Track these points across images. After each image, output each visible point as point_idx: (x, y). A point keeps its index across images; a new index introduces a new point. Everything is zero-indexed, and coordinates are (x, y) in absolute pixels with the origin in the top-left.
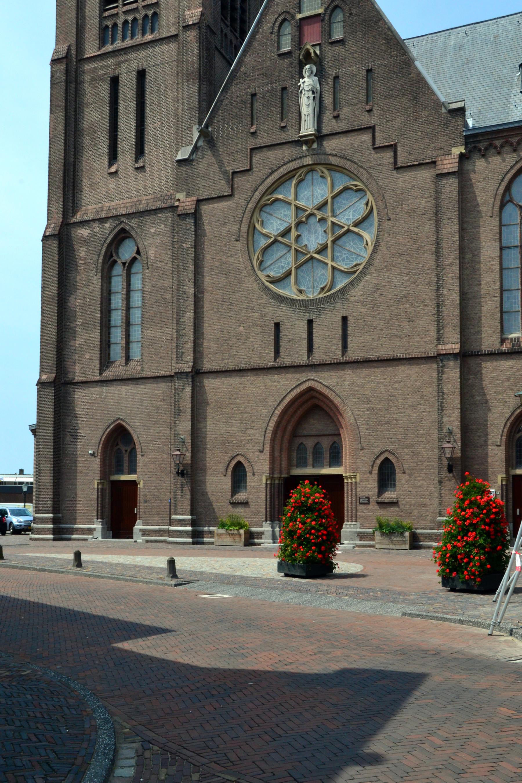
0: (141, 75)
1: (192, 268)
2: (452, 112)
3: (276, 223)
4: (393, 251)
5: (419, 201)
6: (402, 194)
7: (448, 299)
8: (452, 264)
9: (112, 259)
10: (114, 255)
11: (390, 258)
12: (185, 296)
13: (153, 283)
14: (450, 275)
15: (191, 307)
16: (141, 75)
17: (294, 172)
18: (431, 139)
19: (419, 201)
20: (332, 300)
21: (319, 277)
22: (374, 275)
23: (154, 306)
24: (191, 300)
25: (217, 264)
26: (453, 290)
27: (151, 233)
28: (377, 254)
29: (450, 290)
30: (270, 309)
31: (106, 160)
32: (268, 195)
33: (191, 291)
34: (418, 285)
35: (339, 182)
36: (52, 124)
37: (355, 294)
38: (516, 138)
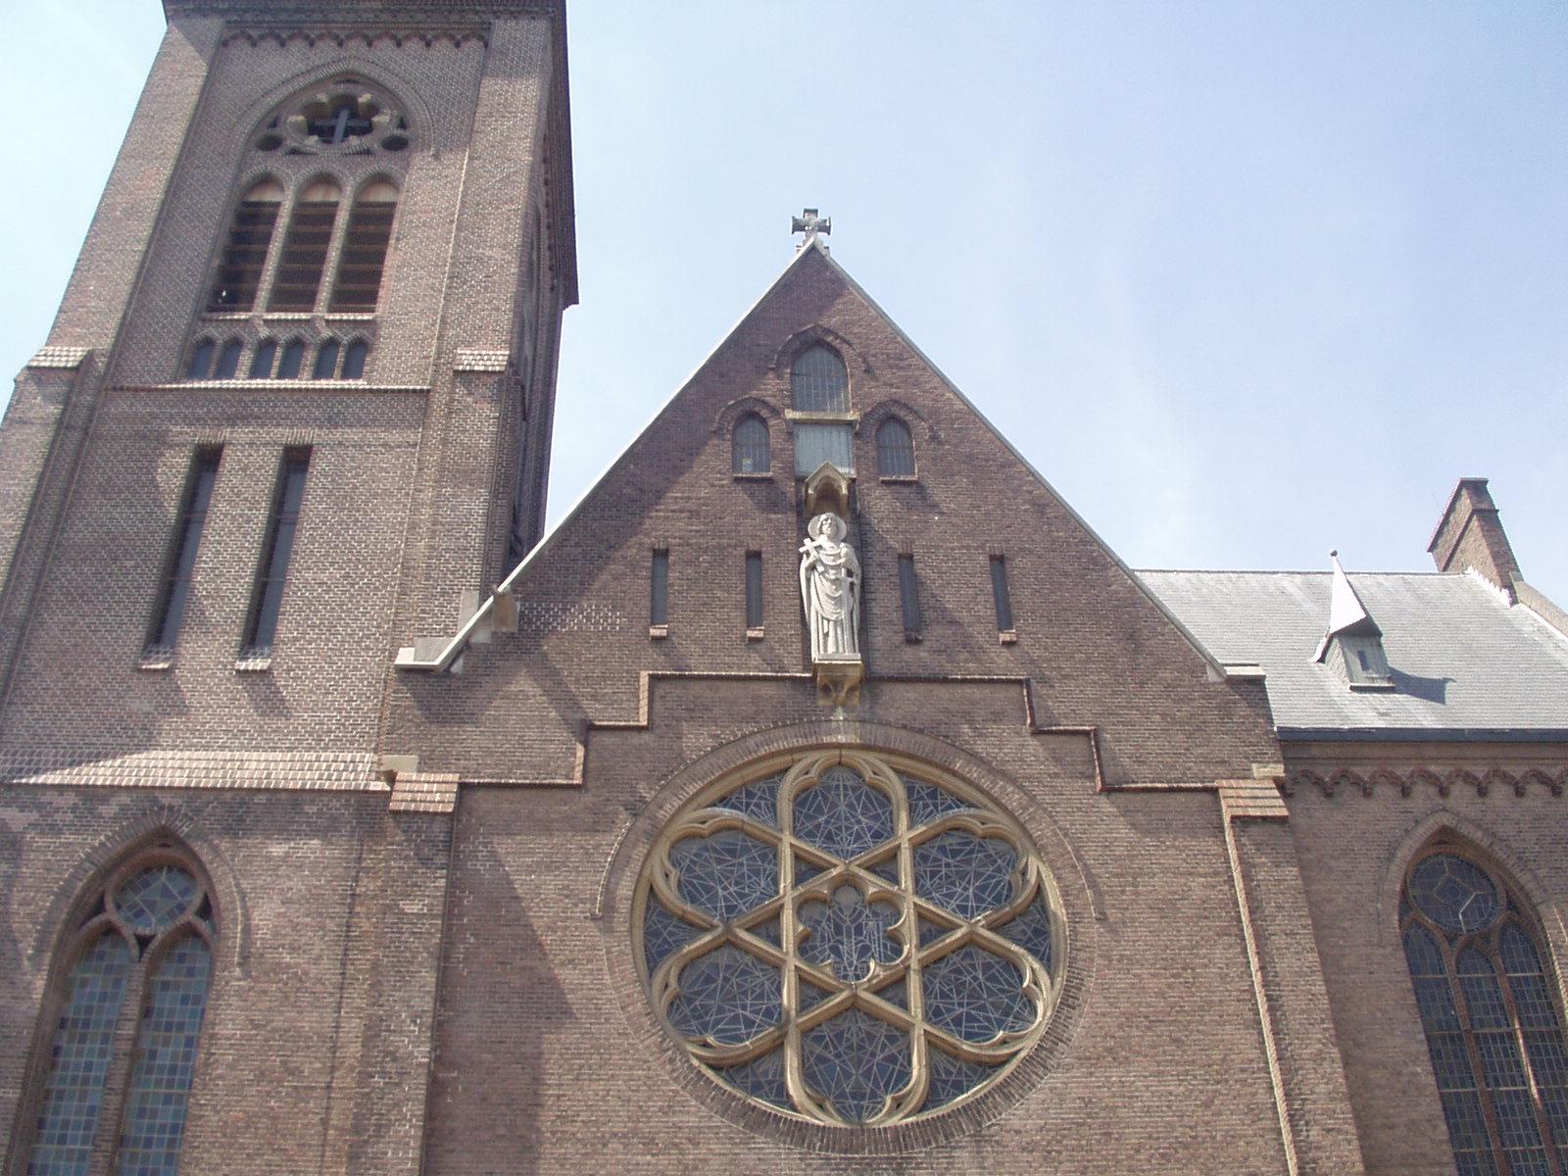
0: (296, 460)
1: (429, 978)
2: (1235, 682)
3: (725, 888)
4: (1124, 1006)
5: (1183, 880)
6: (1131, 857)
7: (1328, 1158)
8: (1319, 1058)
9: (96, 921)
10: (110, 905)
11: (1120, 1027)
12: (390, 1067)
13: (257, 1017)
14: (1322, 1088)
15: (414, 1110)
16: (296, 460)
17: (788, 758)
18: (1190, 735)
19: (1183, 880)
20: (941, 1138)
21: (987, 979)
22: (1075, 1072)
23: (253, 1091)
24: (415, 1088)
25: (516, 981)
26: (1339, 1131)
27: (269, 858)
28: (1077, 1012)
29: (1329, 1131)
30: (716, 1147)
31: (137, 633)
32: (700, 807)
33: (422, 1054)
34: (1219, 1114)
35: (926, 806)
36: (795, 274)
37: (1016, 1123)
38: (1406, 768)
